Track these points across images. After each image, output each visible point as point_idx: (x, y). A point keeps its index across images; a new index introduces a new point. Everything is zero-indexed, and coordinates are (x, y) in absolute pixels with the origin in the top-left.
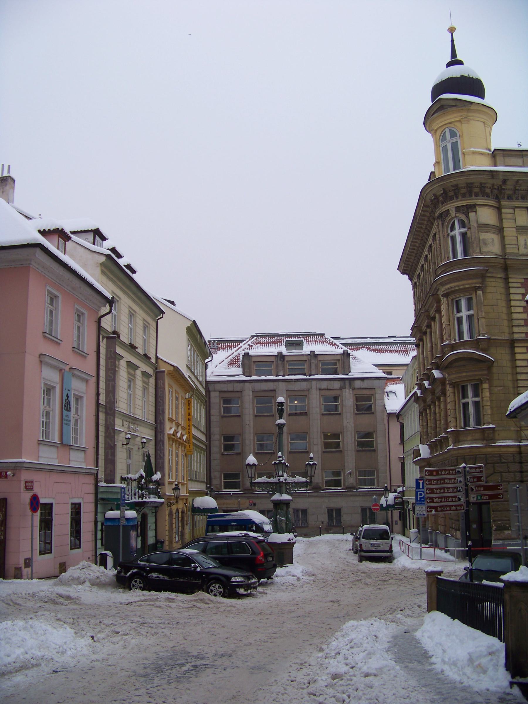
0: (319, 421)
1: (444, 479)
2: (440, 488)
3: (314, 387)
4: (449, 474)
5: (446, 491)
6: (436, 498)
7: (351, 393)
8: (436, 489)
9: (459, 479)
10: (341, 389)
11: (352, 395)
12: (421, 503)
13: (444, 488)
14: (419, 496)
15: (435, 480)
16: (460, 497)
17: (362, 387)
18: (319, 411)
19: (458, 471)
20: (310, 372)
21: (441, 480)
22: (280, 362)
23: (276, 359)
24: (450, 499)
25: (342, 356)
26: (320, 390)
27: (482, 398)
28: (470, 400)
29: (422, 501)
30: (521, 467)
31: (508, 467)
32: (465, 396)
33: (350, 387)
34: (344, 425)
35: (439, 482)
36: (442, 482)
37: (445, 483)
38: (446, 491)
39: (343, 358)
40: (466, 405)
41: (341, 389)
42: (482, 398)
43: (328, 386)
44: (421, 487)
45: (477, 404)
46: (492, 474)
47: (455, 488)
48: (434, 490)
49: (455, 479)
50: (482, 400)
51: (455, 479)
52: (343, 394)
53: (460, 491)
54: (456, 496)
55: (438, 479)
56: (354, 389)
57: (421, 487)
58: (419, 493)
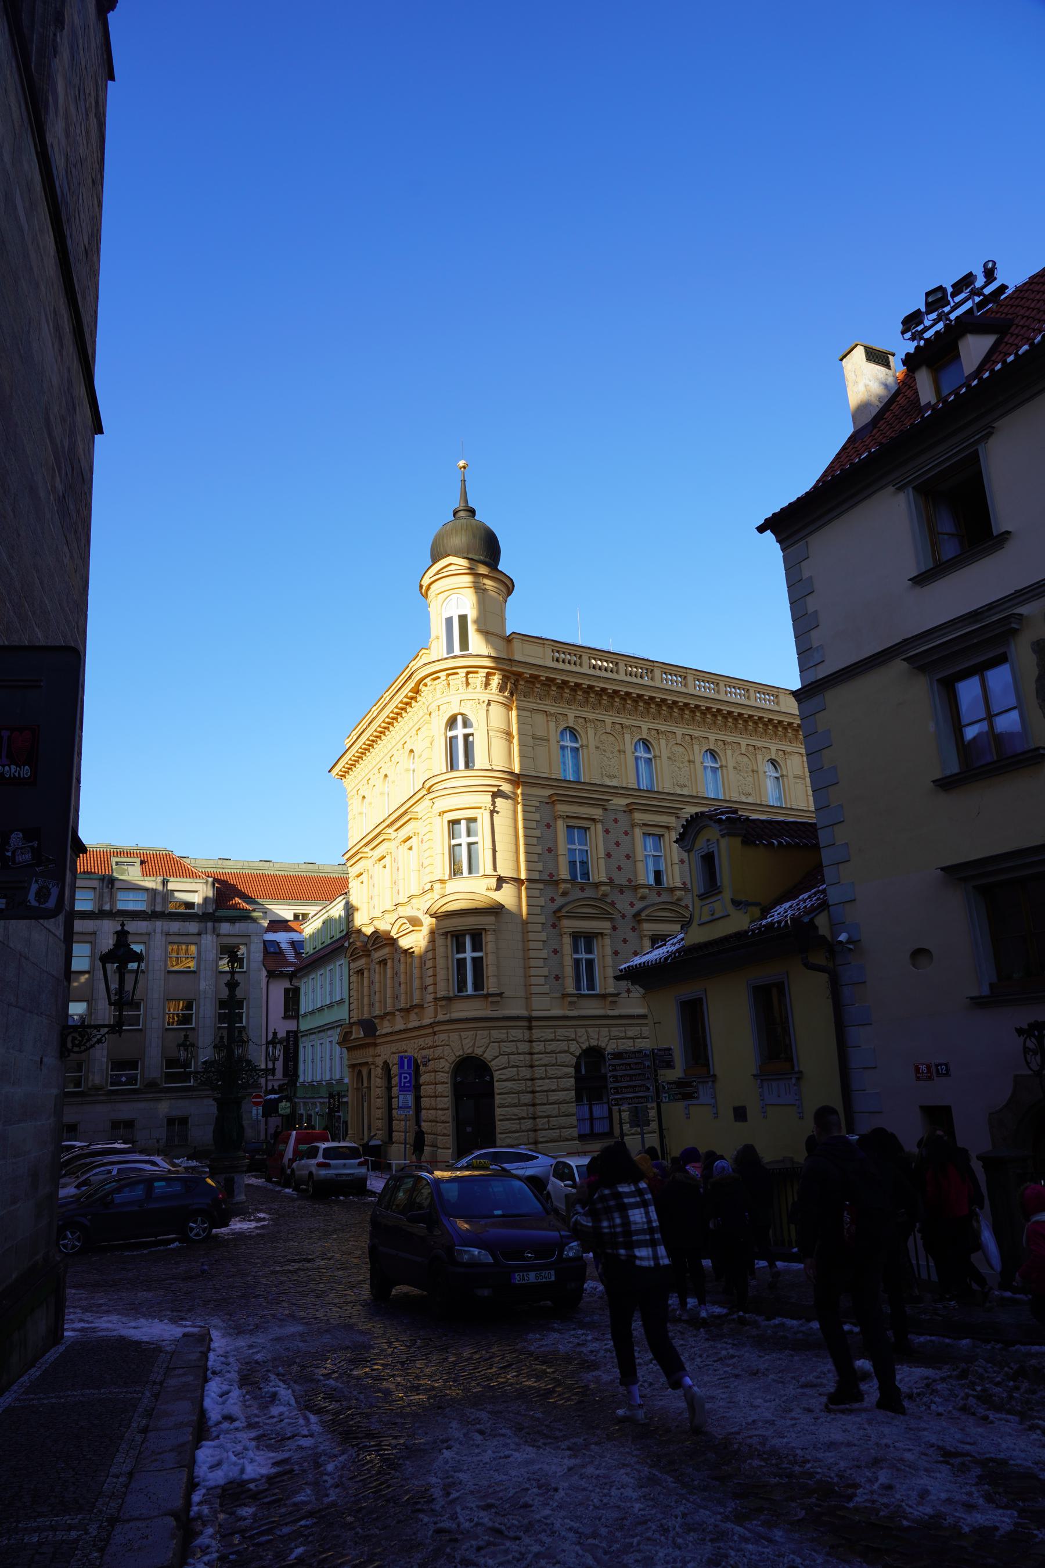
0: (162, 982)
1: (629, 1064)
2: (625, 1076)
3: (158, 930)
4: (636, 1057)
5: (633, 1078)
6: (621, 1087)
7: (215, 940)
8: (621, 1076)
9: (647, 1063)
10: (199, 934)
11: (215, 944)
12: (405, 1089)
13: (630, 1076)
14: (403, 1080)
15: (619, 1065)
16: (649, 1085)
17: (232, 933)
18: (163, 968)
19: (645, 1054)
20: (153, 908)
21: (626, 1065)
22: (106, 890)
23: (101, 884)
24: (637, 1089)
25: (205, 886)
26: (168, 934)
27: (487, 954)
28: (468, 955)
29: (407, 1086)
30: (531, 1047)
31: (517, 1048)
32: (460, 948)
33: (214, 932)
34: (201, 988)
35: (624, 1068)
36: (628, 1067)
37: (631, 1069)
38: (633, 1078)
39: (205, 889)
40: (461, 963)
41: (199, 934)
42: (487, 954)
43: (179, 930)
44: (406, 1067)
45: (477, 963)
46: (498, 1057)
47: (644, 1074)
48: (624, 1068)
49: (642, 1063)
50: (487, 957)
51: (642, 1063)
52: (202, 942)
53: (648, 1078)
54: (644, 1085)
55: (623, 1064)
56: (218, 935)
57: (406, 1067)
58: (403, 1075)
